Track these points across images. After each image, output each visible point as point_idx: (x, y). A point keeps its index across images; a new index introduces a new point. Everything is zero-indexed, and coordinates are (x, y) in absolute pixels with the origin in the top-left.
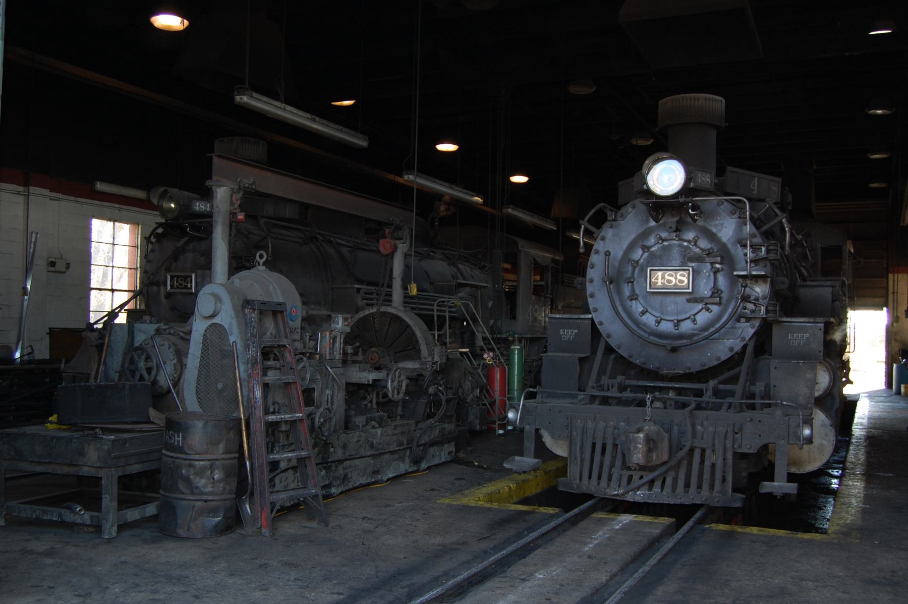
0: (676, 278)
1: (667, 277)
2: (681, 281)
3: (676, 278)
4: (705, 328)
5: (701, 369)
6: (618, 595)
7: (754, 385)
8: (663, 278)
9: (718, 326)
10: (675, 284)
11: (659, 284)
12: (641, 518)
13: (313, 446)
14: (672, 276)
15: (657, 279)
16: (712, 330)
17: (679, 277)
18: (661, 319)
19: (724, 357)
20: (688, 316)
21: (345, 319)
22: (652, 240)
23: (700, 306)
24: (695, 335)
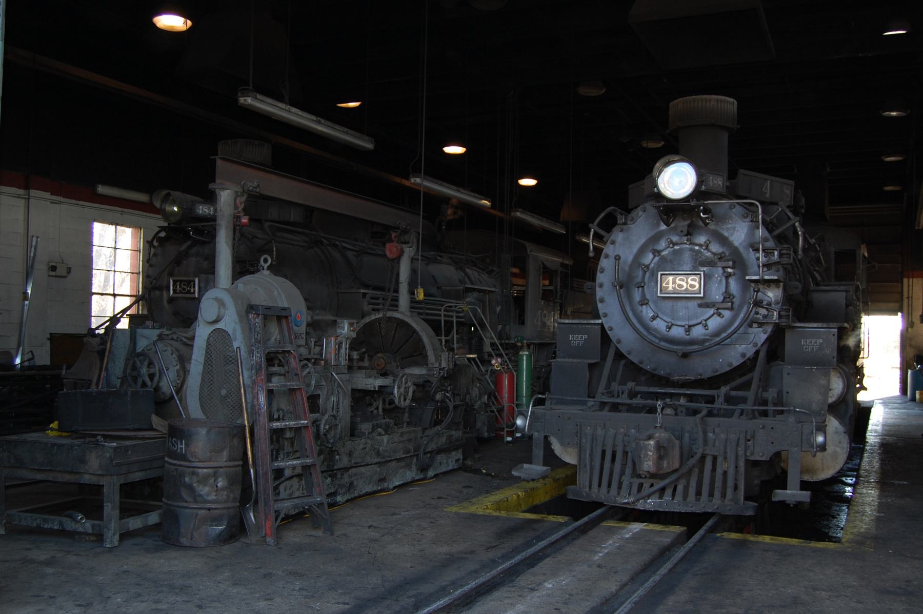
0: (687, 283)
1: (678, 282)
2: (692, 286)
3: (687, 283)
4: (717, 334)
5: (712, 375)
7: (767, 391)
8: (674, 282)
9: (730, 331)
10: (687, 289)
11: (670, 288)
14: (683, 280)
15: (668, 283)
16: (724, 335)
17: (690, 282)
18: (672, 325)
19: (736, 363)
20: (699, 321)
21: (351, 325)
22: (663, 244)
23: (711, 311)
24: (707, 340)
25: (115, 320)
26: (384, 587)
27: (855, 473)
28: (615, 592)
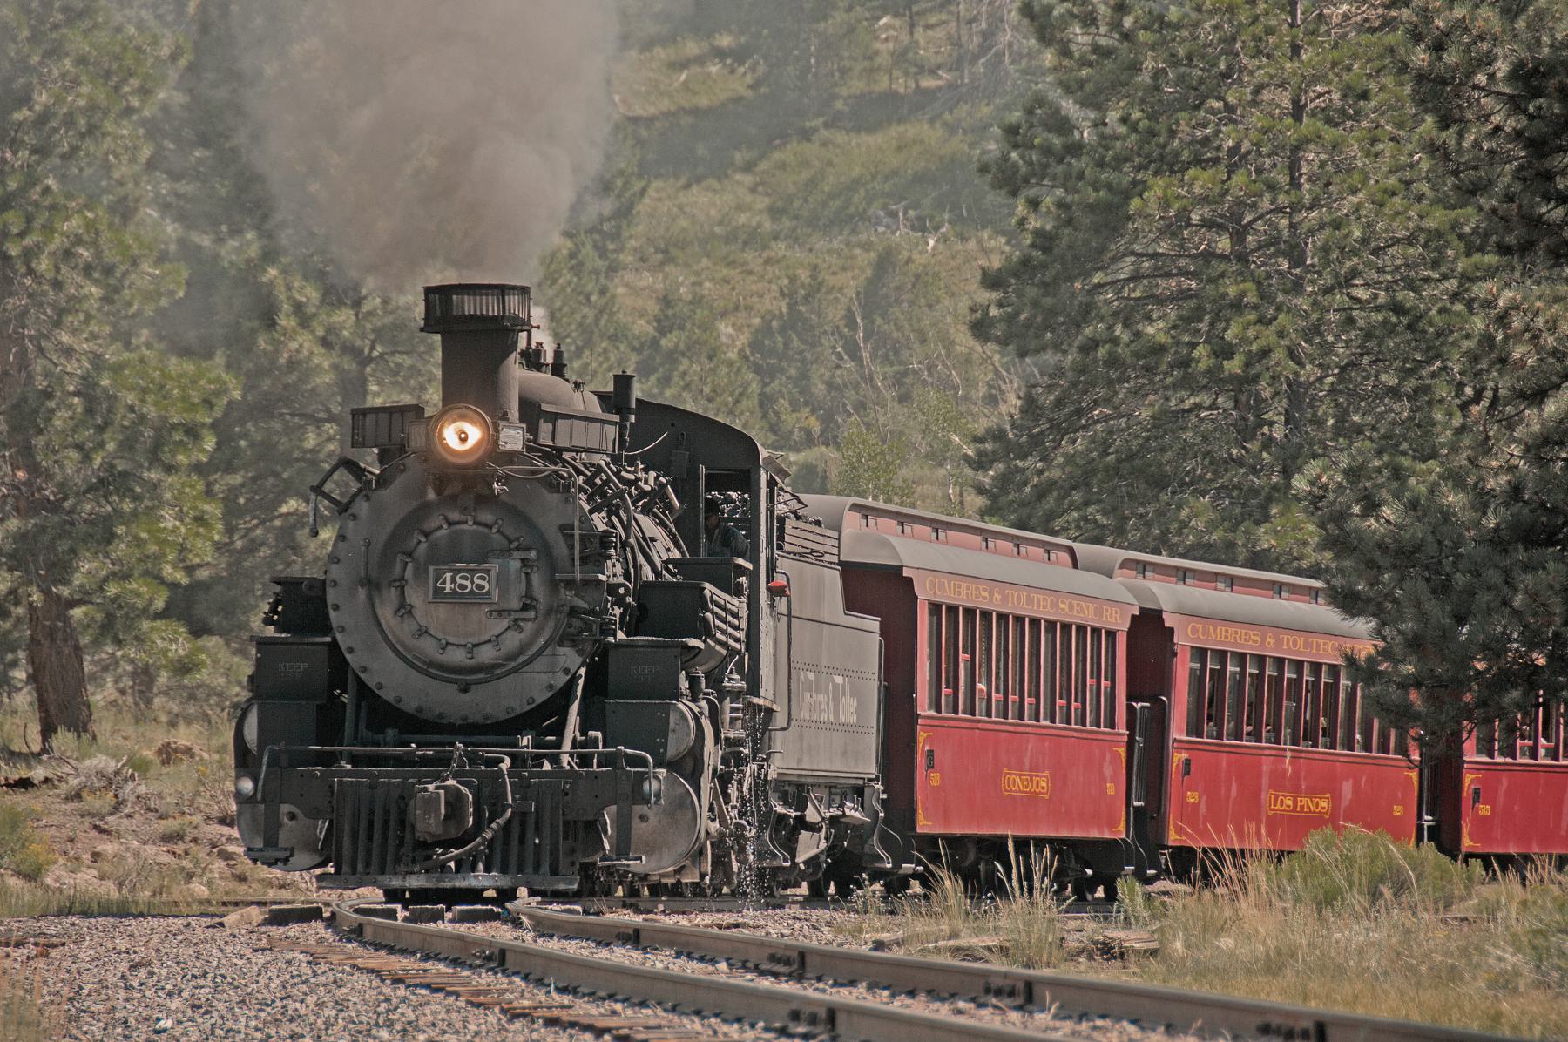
0: (472, 582)
1: (459, 581)
2: (480, 587)
3: (472, 582)
4: (511, 657)
5: (481, 721)
6: (1043, 882)
7: (1525, 572)
8: (453, 581)
9: (530, 653)
10: (472, 590)
11: (448, 590)
12: (1124, 760)
13: (515, 927)
14: (466, 579)
15: (444, 582)
16: (522, 659)
17: (476, 581)
18: (447, 643)
19: (540, 699)
20: (487, 638)
21: (93, 694)
22: (435, 521)
23: (505, 623)
24: (499, 666)
25: (238, 795)
26: (876, 167)
27: (259, 796)
28: (197, 727)
